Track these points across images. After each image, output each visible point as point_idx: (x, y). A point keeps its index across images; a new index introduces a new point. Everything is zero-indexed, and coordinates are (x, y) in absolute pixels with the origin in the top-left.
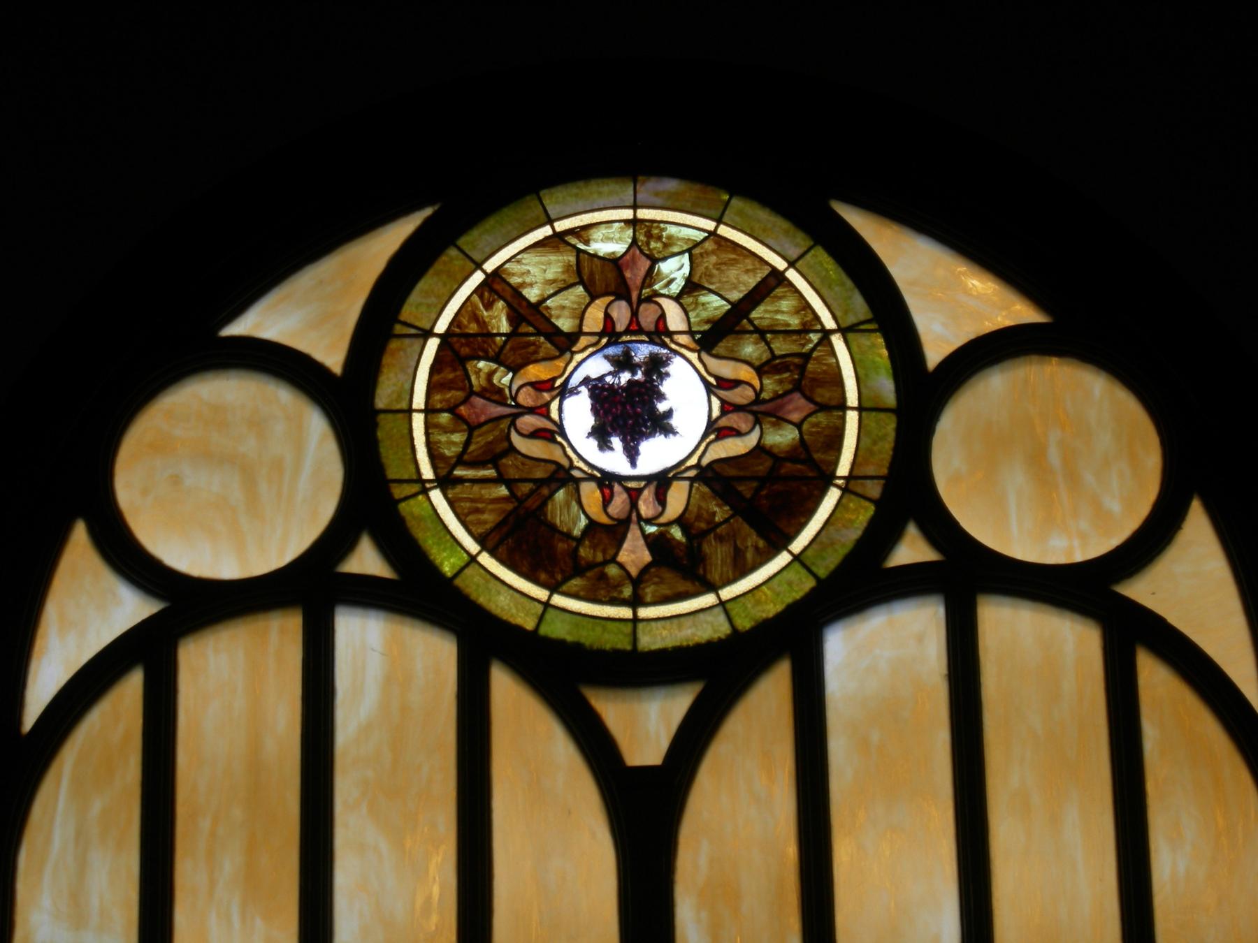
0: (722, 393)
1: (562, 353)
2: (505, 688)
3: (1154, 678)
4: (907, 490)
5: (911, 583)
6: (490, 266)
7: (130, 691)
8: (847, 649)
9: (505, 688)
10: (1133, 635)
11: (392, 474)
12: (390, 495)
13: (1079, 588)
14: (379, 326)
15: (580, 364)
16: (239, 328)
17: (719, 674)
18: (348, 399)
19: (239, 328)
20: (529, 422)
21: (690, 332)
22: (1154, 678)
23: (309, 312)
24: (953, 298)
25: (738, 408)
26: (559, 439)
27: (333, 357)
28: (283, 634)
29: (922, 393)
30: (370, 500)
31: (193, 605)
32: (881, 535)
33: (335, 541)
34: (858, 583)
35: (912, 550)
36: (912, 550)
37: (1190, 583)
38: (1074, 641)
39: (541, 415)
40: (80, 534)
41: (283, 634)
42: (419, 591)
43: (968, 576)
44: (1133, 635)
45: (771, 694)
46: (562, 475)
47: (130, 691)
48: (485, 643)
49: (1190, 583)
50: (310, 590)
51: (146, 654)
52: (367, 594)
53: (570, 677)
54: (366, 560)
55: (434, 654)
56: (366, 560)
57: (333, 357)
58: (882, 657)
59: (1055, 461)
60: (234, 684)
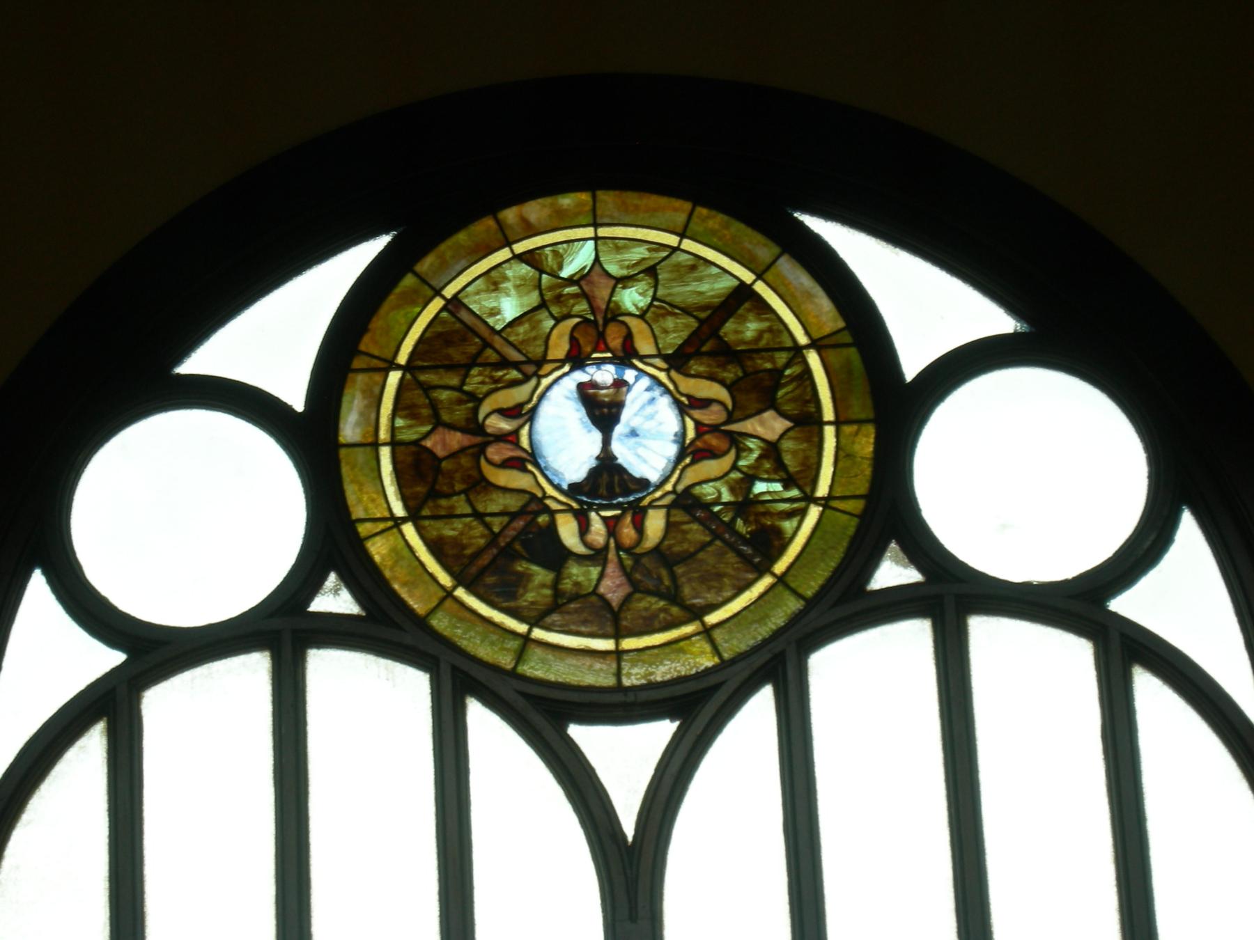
0: (697, 414)
1: (527, 379)
2: (481, 721)
3: (1150, 692)
4: (888, 511)
5: (896, 605)
6: (449, 292)
7: (89, 754)
8: (834, 668)
9: (481, 721)
10: (1127, 652)
11: (357, 513)
12: (356, 533)
13: (1077, 605)
14: (346, 347)
15: (549, 388)
16: (189, 367)
17: (698, 710)
18: (309, 436)
19: (189, 367)
20: (507, 452)
21: (660, 355)
22: (1150, 692)
23: (276, 337)
24: (926, 305)
26: (530, 467)
27: (295, 395)
28: (250, 673)
29: (898, 406)
30: (332, 541)
31: (158, 652)
32: (863, 557)
33: (304, 580)
34: (847, 606)
35: (893, 573)
36: (893, 573)
37: (1182, 596)
38: (1070, 657)
39: (511, 442)
40: (38, 584)
41: (250, 673)
42: (387, 628)
43: (953, 596)
44: (1127, 652)
45: (759, 713)
46: (533, 507)
47: (89, 754)
48: (458, 681)
49: (1182, 596)
50: (280, 630)
51: (109, 708)
52: (337, 633)
53: (545, 717)
54: (334, 600)
55: (406, 690)
56: (334, 600)
57: (295, 395)
58: (872, 681)
59: (1034, 463)
60: (207, 723)
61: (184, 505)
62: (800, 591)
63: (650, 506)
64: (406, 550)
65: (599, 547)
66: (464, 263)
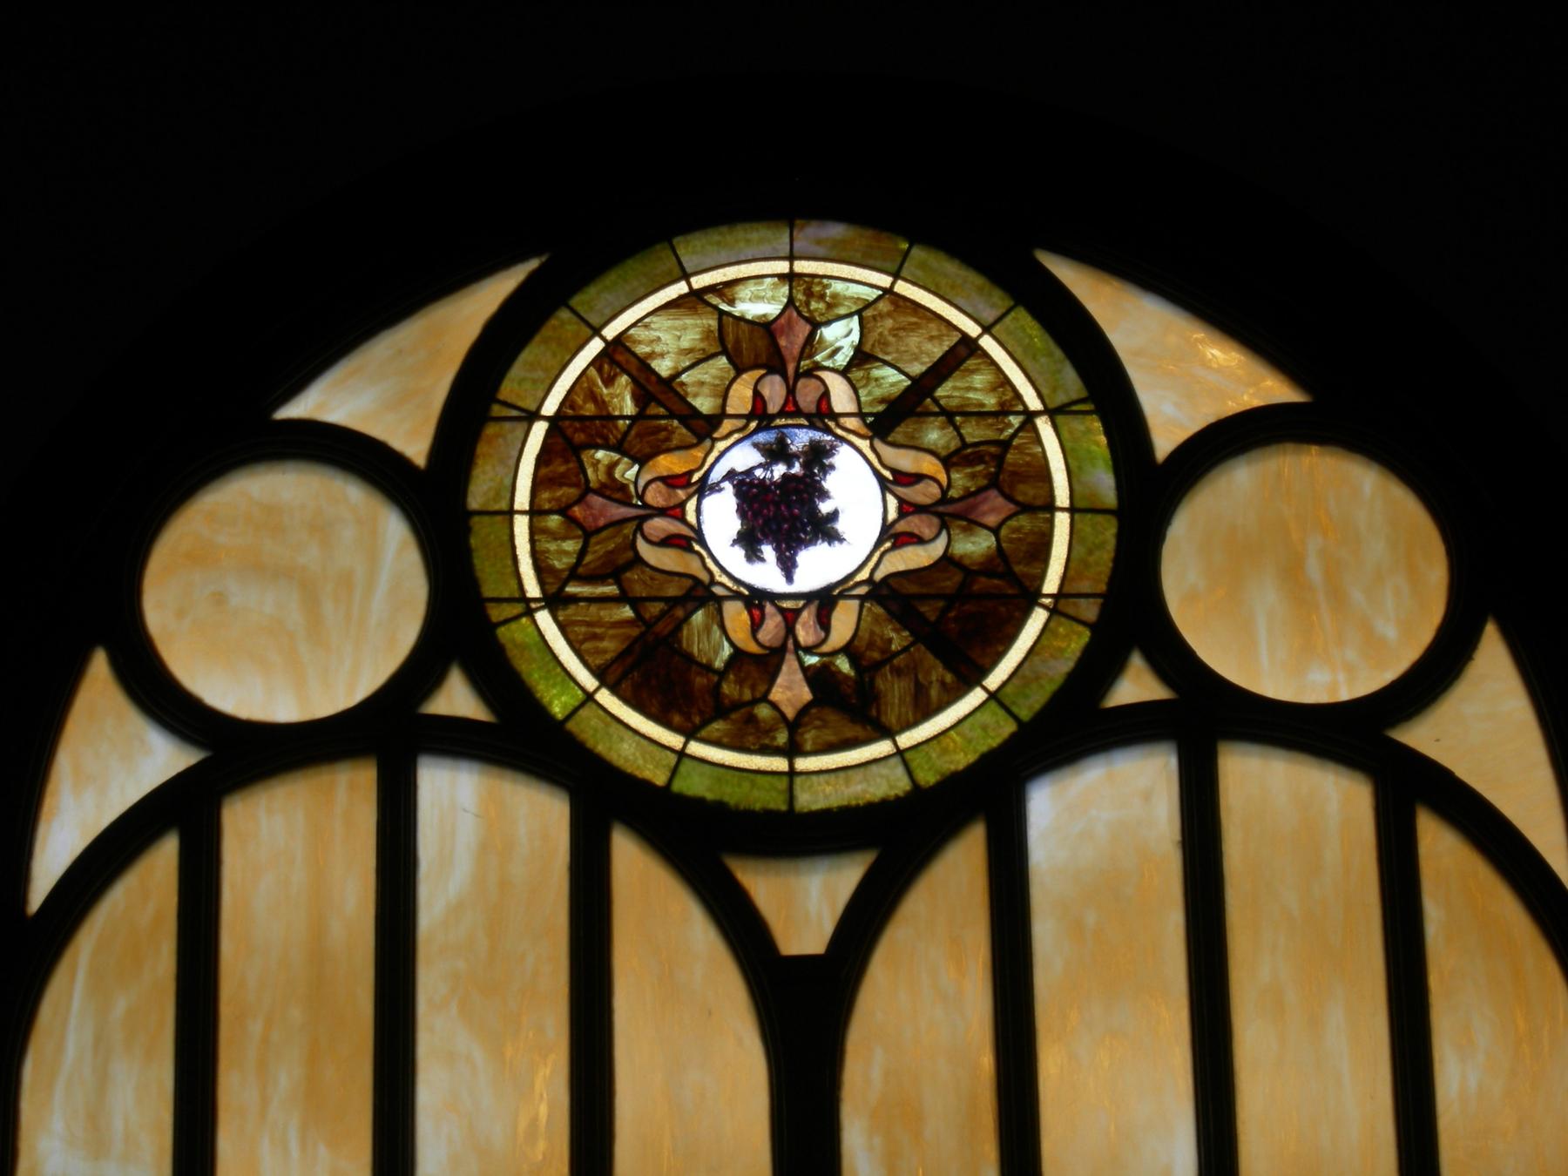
0: (900, 490)
1: (701, 440)
2: (629, 858)
3: (1439, 845)
4: (1130, 611)
5: (1135, 728)
6: (611, 332)
7: (162, 861)
9: (629, 858)
10: (1412, 792)
11: (488, 591)
12: (486, 617)
13: (1344, 733)
15: (722, 454)
16: (298, 409)
18: (434, 498)
19: (298, 409)
20: (660, 526)
21: (860, 415)
22: (1439, 845)
24: (1188, 371)
25: (920, 509)
26: (697, 547)
27: (415, 446)
28: (352, 790)
29: (1150, 490)
30: (461, 624)
31: (241, 755)
32: (1099, 667)
33: (418, 674)
34: (1070, 727)
35: (1136, 686)
36: (1136, 686)
37: (1484, 728)
38: (1338, 800)
39: (675, 517)
40: (100, 666)
41: (352, 790)
42: (523, 737)
43: (1206, 718)
44: (1412, 792)
47: (162, 861)
48: (605, 801)
49: (1484, 728)
50: (386, 735)
51: (182, 816)
52: (457, 741)
54: (456, 698)
55: (541, 815)
56: (456, 698)
57: (415, 446)
58: (1100, 819)
60: (292, 854)
61: (277, 595)
62: (1015, 710)
63: (842, 596)
64: (560, 660)
65: (883, 719)
66: (821, 251)
